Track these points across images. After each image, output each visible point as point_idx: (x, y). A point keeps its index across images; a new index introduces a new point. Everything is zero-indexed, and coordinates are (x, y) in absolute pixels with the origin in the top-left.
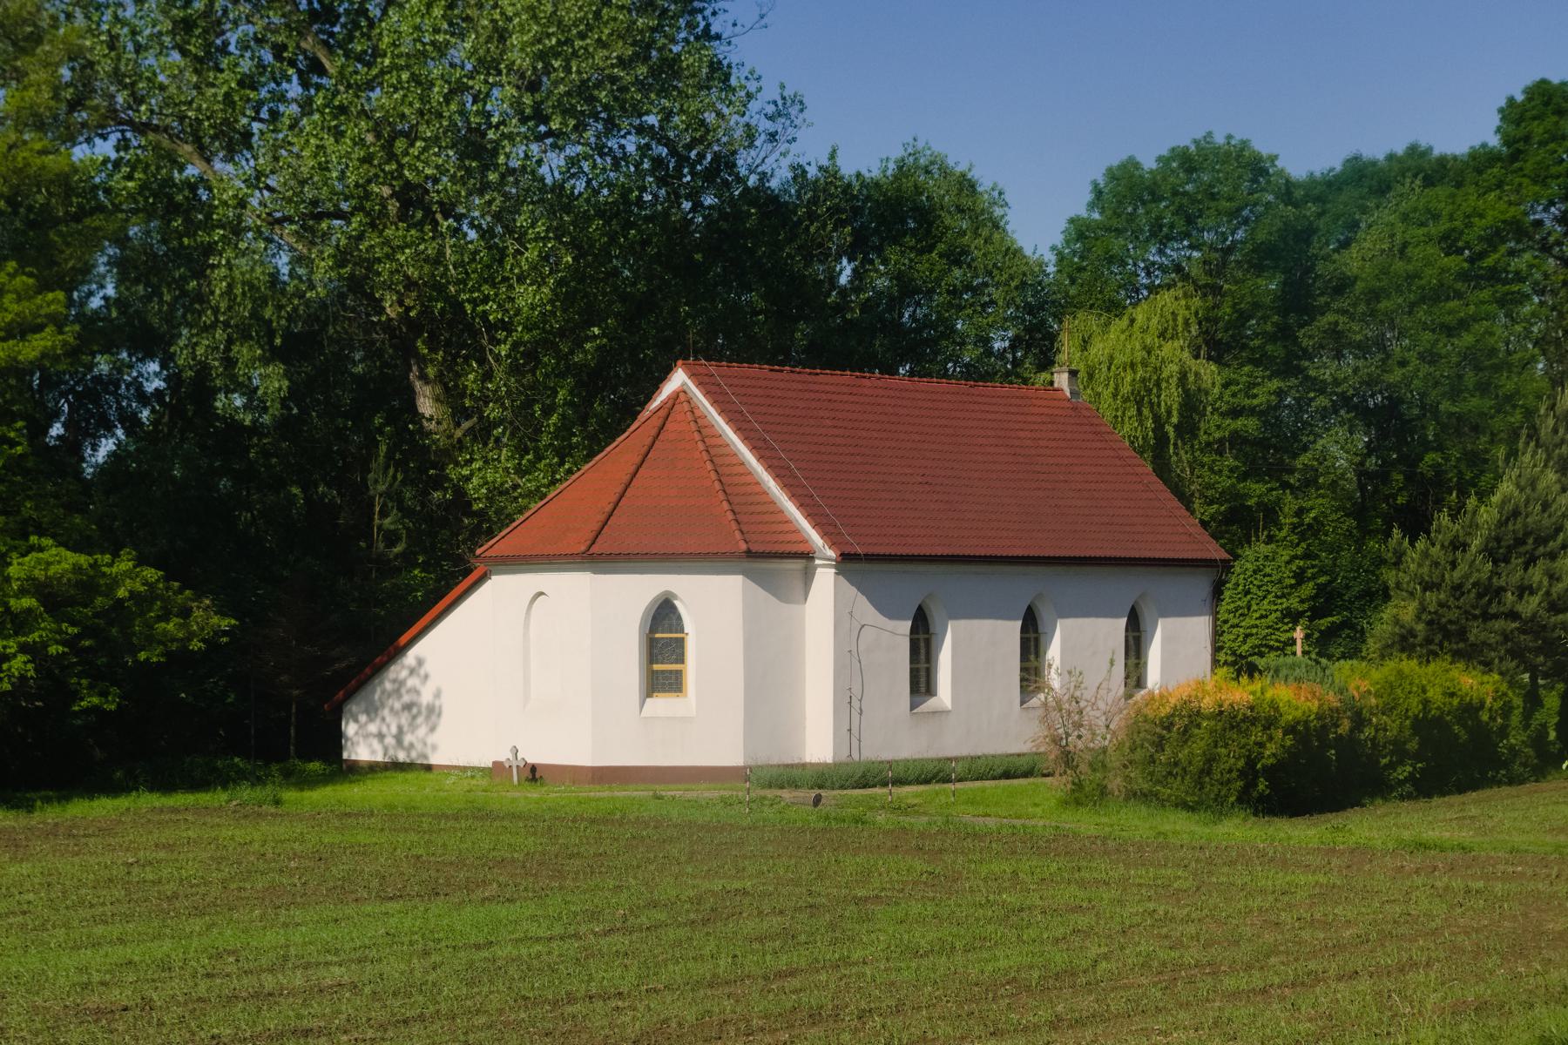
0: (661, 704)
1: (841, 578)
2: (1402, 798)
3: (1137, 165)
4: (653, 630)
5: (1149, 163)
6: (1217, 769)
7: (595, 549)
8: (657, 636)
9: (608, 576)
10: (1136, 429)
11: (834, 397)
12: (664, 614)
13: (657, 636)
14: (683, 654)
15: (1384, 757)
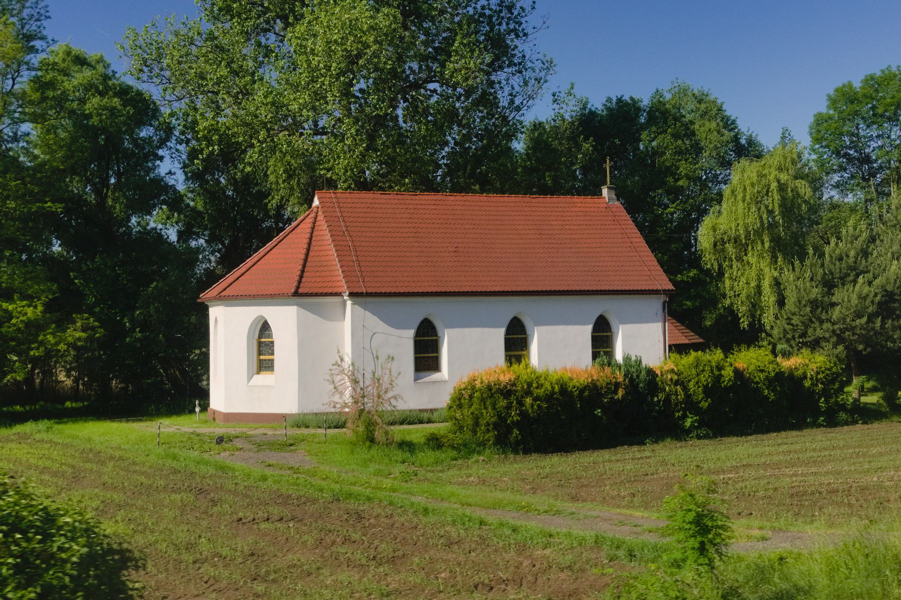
0: (264, 379)
1: (357, 306)
2: (699, 437)
3: (850, 85)
4: (260, 337)
5: (857, 84)
6: (482, 422)
7: (300, 291)
8: (262, 340)
9: (287, 307)
10: (756, 219)
11: (418, 207)
12: (265, 328)
13: (262, 340)
14: (273, 351)
15: (678, 411)
